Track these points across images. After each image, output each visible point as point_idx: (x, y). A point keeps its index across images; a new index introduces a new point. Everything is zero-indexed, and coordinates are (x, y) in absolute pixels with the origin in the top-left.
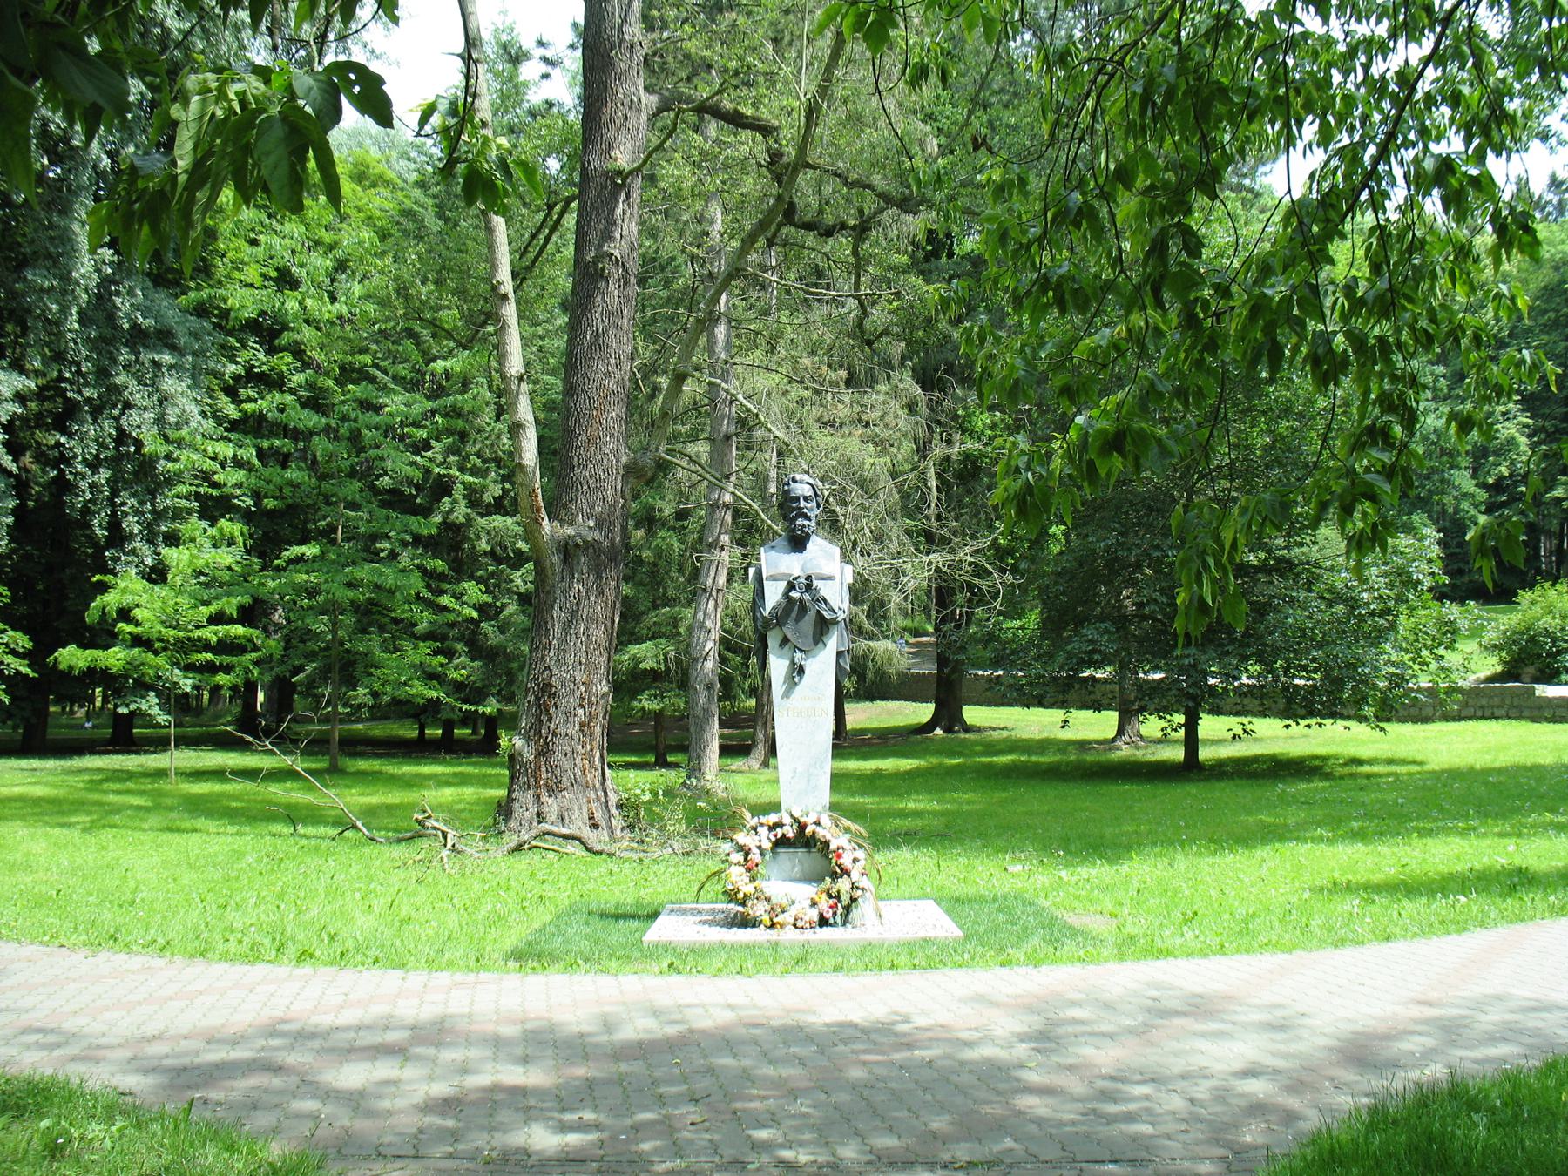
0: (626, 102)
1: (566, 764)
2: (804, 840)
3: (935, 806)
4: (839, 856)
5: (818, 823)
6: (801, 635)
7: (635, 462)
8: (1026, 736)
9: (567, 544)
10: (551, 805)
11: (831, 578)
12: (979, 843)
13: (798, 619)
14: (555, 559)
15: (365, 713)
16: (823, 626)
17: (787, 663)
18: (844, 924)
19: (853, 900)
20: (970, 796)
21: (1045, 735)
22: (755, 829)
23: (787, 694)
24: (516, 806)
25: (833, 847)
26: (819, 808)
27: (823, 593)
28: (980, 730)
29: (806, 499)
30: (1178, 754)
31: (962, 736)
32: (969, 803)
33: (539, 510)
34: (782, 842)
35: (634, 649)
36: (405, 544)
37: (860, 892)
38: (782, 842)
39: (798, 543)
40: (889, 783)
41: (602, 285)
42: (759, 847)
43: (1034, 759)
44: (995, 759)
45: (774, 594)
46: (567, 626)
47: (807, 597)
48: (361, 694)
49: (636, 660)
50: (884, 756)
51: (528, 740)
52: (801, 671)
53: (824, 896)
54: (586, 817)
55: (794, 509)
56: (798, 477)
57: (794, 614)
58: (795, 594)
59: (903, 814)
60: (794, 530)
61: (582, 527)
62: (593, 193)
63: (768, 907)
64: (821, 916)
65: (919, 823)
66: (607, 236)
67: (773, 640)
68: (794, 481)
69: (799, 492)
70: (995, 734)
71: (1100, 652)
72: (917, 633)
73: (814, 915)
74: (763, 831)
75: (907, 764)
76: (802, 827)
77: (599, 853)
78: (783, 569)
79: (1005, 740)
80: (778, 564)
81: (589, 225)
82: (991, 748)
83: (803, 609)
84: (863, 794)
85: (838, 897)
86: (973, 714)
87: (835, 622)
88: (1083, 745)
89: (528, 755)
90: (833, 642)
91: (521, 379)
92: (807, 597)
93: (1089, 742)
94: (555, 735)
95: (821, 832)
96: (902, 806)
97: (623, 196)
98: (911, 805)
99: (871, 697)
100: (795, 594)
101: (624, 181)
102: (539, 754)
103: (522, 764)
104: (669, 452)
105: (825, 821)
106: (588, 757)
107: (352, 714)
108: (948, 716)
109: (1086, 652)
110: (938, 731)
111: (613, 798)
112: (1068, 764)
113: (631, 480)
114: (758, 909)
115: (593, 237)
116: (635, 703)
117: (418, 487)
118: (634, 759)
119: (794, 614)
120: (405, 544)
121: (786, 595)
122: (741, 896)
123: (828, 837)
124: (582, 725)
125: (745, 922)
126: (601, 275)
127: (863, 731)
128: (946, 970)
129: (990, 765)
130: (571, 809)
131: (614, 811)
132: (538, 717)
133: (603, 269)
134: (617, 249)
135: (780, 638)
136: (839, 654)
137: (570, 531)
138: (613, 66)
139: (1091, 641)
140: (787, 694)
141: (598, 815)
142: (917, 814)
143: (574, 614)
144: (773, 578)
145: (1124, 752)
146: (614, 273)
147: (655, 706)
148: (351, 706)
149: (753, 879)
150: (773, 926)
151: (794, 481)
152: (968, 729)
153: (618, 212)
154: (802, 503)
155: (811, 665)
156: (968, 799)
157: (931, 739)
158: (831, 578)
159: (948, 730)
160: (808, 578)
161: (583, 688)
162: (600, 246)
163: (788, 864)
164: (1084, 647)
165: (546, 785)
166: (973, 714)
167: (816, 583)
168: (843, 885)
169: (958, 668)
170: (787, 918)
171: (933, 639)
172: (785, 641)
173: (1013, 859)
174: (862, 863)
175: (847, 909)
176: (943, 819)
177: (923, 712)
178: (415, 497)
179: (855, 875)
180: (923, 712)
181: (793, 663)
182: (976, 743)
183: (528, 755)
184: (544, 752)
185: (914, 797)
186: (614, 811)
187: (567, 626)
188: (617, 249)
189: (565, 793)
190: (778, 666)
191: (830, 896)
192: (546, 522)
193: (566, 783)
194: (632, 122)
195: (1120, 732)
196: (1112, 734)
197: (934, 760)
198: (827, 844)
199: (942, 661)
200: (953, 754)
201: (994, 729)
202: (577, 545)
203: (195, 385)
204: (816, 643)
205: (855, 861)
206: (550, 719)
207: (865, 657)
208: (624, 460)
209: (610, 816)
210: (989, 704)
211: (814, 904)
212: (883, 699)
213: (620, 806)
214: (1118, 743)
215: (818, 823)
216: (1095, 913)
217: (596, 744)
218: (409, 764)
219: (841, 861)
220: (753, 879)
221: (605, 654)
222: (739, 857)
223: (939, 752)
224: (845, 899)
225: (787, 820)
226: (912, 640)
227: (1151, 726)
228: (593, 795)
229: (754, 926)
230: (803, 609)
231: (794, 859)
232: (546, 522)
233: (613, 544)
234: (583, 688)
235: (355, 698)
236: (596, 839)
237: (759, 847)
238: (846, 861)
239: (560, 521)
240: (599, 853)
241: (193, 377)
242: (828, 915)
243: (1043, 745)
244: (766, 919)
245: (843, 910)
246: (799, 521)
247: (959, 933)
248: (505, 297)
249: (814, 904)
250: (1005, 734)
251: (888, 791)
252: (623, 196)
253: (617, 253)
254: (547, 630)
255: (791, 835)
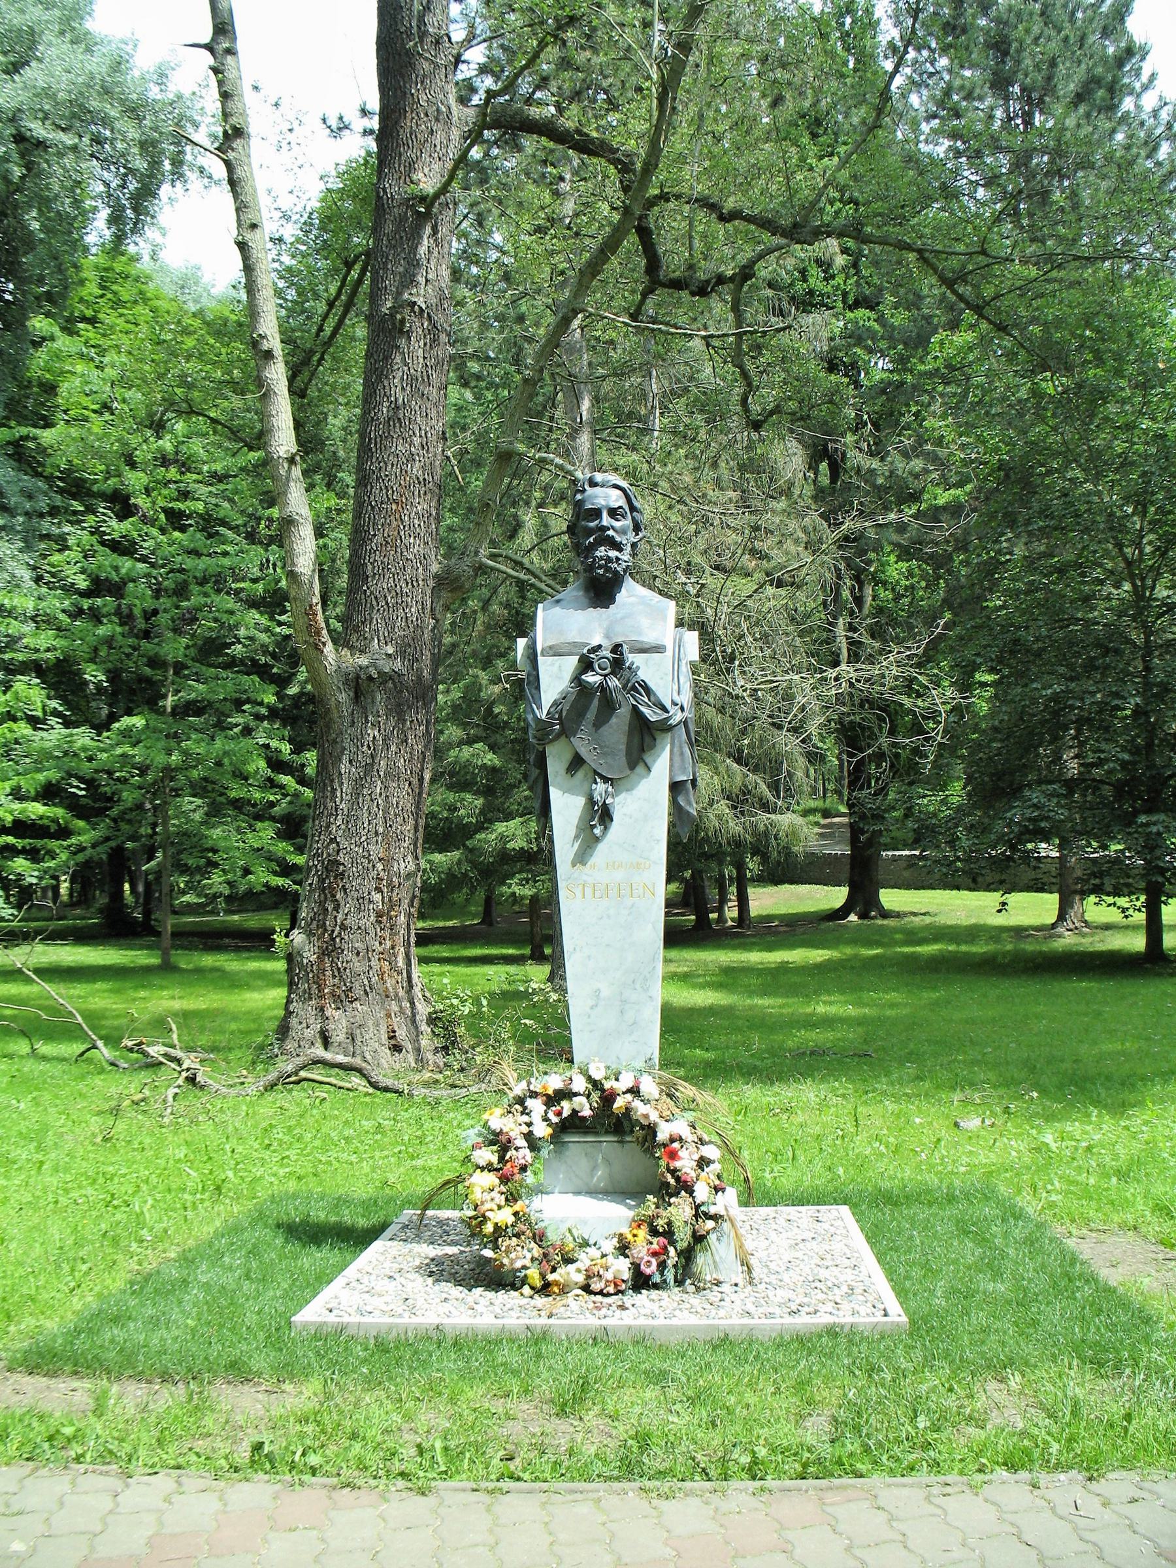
0: (432, 111)
1: (358, 966)
2: (608, 1121)
3: (851, 1011)
4: (673, 1155)
5: (634, 1091)
6: (604, 751)
7: (448, 570)
8: (951, 922)
9: (358, 677)
10: (339, 1022)
11: (658, 649)
12: (911, 1069)
13: (599, 723)
14: (343, 697)
15: (221, 904)
16: (644, 735)
17: (580, 802)
18: (679, 1282)
19: (699, 1238)
20: (892, 996)
21: (973, 921)
22: (521, 1101)
23: (581, 858)
24: (294, 1021)
25: (662, 1136)
26: (640, 1064)
27: (642, 675)
28: (898, 915)
29: (613, 513)
30: (1138, 943)
31: (880, 922)
32: (893, 1005)
33: (318, 633)
34: (571, 1125)
35: (501, 827)
36: (259, 718)
37: (710, 1224)
38: (571, 1125)
39: (602, 591)
40: (796, 979)
41: (402, 342)
42: (529, 1136)
43: (964, 948)
44: (918, 949)
45: (555, 681)
46: (359, 785)
47: (614, 682)
48: (216, 881)
49: (503, 838)
50: (792, 946)
51: (310, 934)
52: (606, 816)
53: (643, 1233)
54: (384, 1037)
55: (589, 532)
56: (599, 477)
57: (591, 715)
58: (591, 678)
59: (811, 1023)
60: (590, 568)
61: (379, 654)
62: (389, 227)
63: (537, 1252)
64: (636, 1268)
65: (830, 1035)
66: (409, 280)
67: (555, 766)
68: (593, 484)
69: (601, 502)
70: (917, 919)
71: (1047, 818)
72: (826, 814)
73: (621, 1267)
74: (536, 1106)
75: (818, 955)
76: (608, 1098)
77: (386, 1089)
78: (573, 636)
79: (928, 927)
80: (564, 629)
81: (385, 269)
82: (913, 937)
83: (608, 705)
84: (764, 993)
85: (669, 1234)
86: (890, 898)
87: (665, 727)
88: (1019, 932)
89: (310, 955)
90: (661, 766)
91: (291, 461)
92: (614, 682)
93: (1026, 929)
94: (343, 927)
95: (640, 1108)
96: (809, 1010)
97: (428, 230)
98: (821, 1009)
99: (776, 881)
100: (591, 678)
101: (429, 208)
102: (324, 953)
103: (302, 967)
104: (493, 557)
105: (649, 1087)
106: (389, 956)
107: (207, 905)
108: (863, 899)
109: (1030, 820)
110: (853, 918)
111: (423, 1010)
112: (1005, 954)
113: (444, 594)
114: (520, 1256)
115: (390, 283)
116: (504, 889)
117: (274, 656)
118: (511, 951)
119: (591, 715)
120: (259, 718)
121: (577, 679)
122: (489, 1228)
123: (654, 1117)
124: (379, 915)
125: (498, 1279)
126: (400, 330)
127: (769, 918)
128: (877, 1480)
129: (914, 957)
130: (366, 1025)
131: (424, 1027)
132: (321, 904)
133: (403, 321)
134: (421, 296)
135: (568, 757)
136: (676, 788)
137: (363, 661)
138: (412, 65)
139: (1036, 806)
140: (581, 858)
141: (402, 1033)
142: (828, 1022)
143: (369, 768)
144: (555, 651)
145: (1067, 941)
146: (418, 327)
147: (528, 891)
148: (206, 896)
149: (511, 1198)
150: (545, 1289)
151: (593, 484)
152: (885, 914)
153: (422, 250)
154: (606, 520)
155: (624, 806)
156: (893, 1001)
157: (844, 926)
158: (658, 649)
159: (863, 916)
160: (617, 648)
161: (380, 866)
162: (399, 294)
163: (584, 1164)
164: (1029, 813)
165: (333, 994)
166: (890, 898)
167: (631, 658)
168: (680, 1211)
169: (874, 843)
170: (571, 1274)
171: (845, 820)
172: (577, 762)
173: (965, 1102)
174: (715, 1168)
175: (687, 1255)
176: (860, 1030)
177: (836, 896)
178: (273, 667)
179: (702, 1192)
180: (836, 896)
181: (591, 801)
182: (895, 930)
183: (310, 955)
184: (330, 951)
185: (825, 998)
186: (424, 1027)
187: (359, 785)
188: (421, 296)
189: (357, 1004)
190: (566, 807)
191: (654, 1232)
192: (329, 649)
193: (358, 992)
194: (439, 138)
195: (1062, 917)
196: (1051, 918)
197: (849, 951)
198: (651, 1130)
199: (854, 841)
200: (870, 944)
201: (915, 914)
202: (370, 678)
203: (28, 548)
204: (632, 766)
205: (703, 1163)
206: (337, 908)
207: (766, 833)
208: (435, 568)
209: (419, 1033)
210: (908, 887)
211: (623, 1248)
212: (792, 883)
213: (432, 1020)
214: (1060, 930)
215: (634, 1091)
216: (1123, 1226)
217: (400, 940)
218: (255, 959)
219: (677, 1164)
220: (511, 1198)
221: (411, 822)
222: (488, 1155)
223: (854, 942)
224: (683, 1236)
225: (580, 1084)
226: (823, 822)
227: (1096, 910)
228: (395, 1007)
229: (514, 1287)
230: (608, 705)
231: (594, 1156)
232: (329, 649)
233: (420, 677)
234: (380, 866)
235: (211, 886)
236: (386, 1067)
237: (529, 1136)
238: (686, 1163)
239: (351, 648)
240: (386, 1089)
241: (25, 540)
242: (651, 1269)
243: (973, 933)
244: (533, 1274)
245: (677, 1261)
246: (601, 552)
247: (898, 1314)
248: (269, 355)
249: (623, 1248)
250: (928, 920)
251: (793, 990)
252: (428, 230)
253: (421, 302)
254: (334, 791)
255: (586, 1112)
